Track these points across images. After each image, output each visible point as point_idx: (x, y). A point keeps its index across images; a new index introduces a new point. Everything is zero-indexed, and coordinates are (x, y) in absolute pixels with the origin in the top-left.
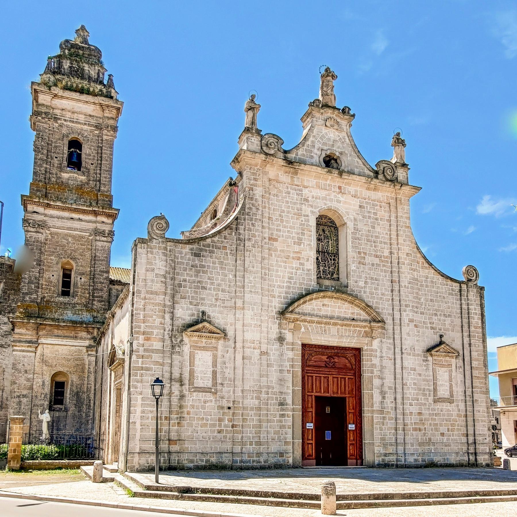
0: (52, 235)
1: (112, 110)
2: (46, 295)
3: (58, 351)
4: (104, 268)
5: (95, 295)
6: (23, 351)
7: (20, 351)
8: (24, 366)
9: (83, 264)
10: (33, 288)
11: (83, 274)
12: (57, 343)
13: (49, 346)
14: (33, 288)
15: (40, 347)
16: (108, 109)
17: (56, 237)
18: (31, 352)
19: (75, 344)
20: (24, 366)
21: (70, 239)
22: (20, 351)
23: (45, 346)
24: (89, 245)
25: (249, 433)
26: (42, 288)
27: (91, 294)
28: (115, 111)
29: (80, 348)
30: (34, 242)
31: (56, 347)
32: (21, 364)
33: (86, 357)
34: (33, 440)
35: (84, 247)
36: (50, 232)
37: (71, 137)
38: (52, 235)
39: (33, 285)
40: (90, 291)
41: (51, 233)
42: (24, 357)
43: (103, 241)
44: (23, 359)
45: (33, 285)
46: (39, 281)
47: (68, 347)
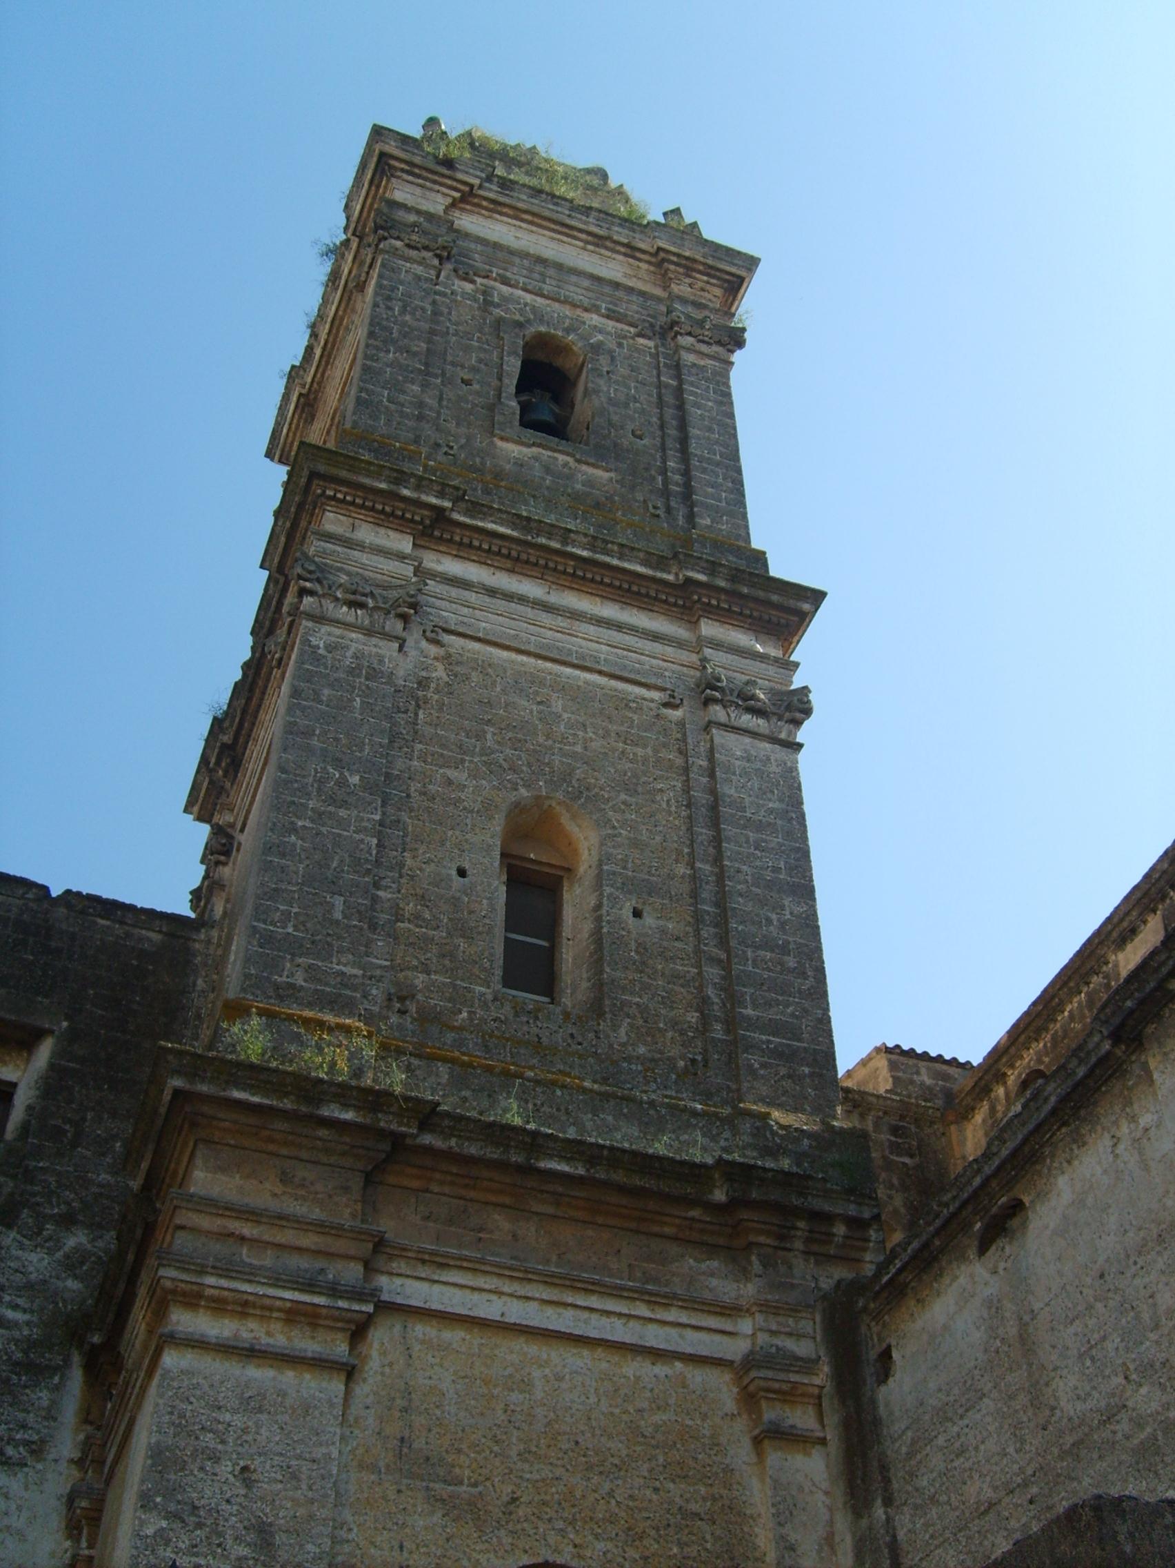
0: (458, 669)
1: (708, 287)
2: (420, 980)
3: (526, 1385)
4: (776, 870)
5: (749, 1012)
6: (252, 1353)
7: (226, 1349)
8: (249, 1484)
9: (644, 836)
10: (338, 915)
11: (652, 890)
12: (516, 1312)
13: (454, 1336)
14: (338, 915)
15: (382, 1337)
16: (688, 280)
17: (475, 676)
18: (319, 1364)
19: (654, 1337)
20: (249, 1484)
21: (558, 705)
22: (226, 1349)
23: (420, 1329)
24: (665, 745)
25: (181, 1218)
26: (395, 937)
27: (717, 1010)
28: (718, 292)
29: (698, 1377)
30: (351, 671)
31: (514, 1350)
32: (225, 1469)
33: (741, 1453)
34: (498, 1133)
35: (640, 751)
36: (442, 652)
37: (531, 330)
38: (458, 669)
39: (339, 901)
40: (710, 992)
41: (449, 656)
42: (253, 1403)
43: (754, 734)
44: (238, 1420)
45: (339, 901)
46: (377, 886)
47: (600, 1362)
